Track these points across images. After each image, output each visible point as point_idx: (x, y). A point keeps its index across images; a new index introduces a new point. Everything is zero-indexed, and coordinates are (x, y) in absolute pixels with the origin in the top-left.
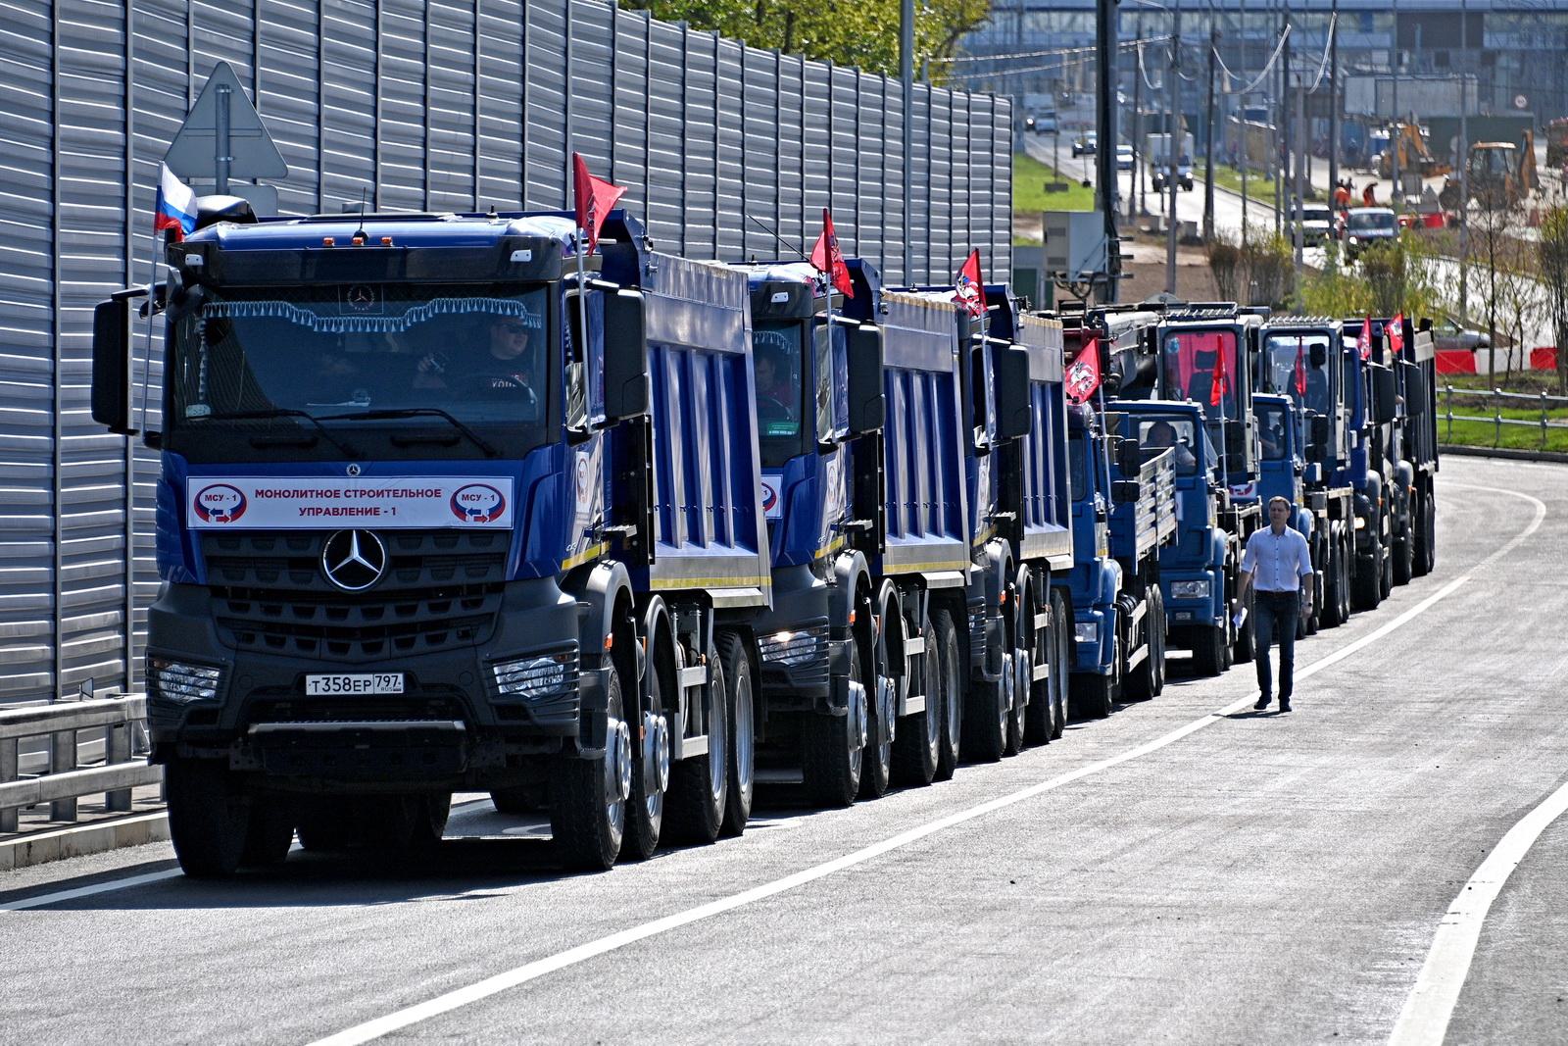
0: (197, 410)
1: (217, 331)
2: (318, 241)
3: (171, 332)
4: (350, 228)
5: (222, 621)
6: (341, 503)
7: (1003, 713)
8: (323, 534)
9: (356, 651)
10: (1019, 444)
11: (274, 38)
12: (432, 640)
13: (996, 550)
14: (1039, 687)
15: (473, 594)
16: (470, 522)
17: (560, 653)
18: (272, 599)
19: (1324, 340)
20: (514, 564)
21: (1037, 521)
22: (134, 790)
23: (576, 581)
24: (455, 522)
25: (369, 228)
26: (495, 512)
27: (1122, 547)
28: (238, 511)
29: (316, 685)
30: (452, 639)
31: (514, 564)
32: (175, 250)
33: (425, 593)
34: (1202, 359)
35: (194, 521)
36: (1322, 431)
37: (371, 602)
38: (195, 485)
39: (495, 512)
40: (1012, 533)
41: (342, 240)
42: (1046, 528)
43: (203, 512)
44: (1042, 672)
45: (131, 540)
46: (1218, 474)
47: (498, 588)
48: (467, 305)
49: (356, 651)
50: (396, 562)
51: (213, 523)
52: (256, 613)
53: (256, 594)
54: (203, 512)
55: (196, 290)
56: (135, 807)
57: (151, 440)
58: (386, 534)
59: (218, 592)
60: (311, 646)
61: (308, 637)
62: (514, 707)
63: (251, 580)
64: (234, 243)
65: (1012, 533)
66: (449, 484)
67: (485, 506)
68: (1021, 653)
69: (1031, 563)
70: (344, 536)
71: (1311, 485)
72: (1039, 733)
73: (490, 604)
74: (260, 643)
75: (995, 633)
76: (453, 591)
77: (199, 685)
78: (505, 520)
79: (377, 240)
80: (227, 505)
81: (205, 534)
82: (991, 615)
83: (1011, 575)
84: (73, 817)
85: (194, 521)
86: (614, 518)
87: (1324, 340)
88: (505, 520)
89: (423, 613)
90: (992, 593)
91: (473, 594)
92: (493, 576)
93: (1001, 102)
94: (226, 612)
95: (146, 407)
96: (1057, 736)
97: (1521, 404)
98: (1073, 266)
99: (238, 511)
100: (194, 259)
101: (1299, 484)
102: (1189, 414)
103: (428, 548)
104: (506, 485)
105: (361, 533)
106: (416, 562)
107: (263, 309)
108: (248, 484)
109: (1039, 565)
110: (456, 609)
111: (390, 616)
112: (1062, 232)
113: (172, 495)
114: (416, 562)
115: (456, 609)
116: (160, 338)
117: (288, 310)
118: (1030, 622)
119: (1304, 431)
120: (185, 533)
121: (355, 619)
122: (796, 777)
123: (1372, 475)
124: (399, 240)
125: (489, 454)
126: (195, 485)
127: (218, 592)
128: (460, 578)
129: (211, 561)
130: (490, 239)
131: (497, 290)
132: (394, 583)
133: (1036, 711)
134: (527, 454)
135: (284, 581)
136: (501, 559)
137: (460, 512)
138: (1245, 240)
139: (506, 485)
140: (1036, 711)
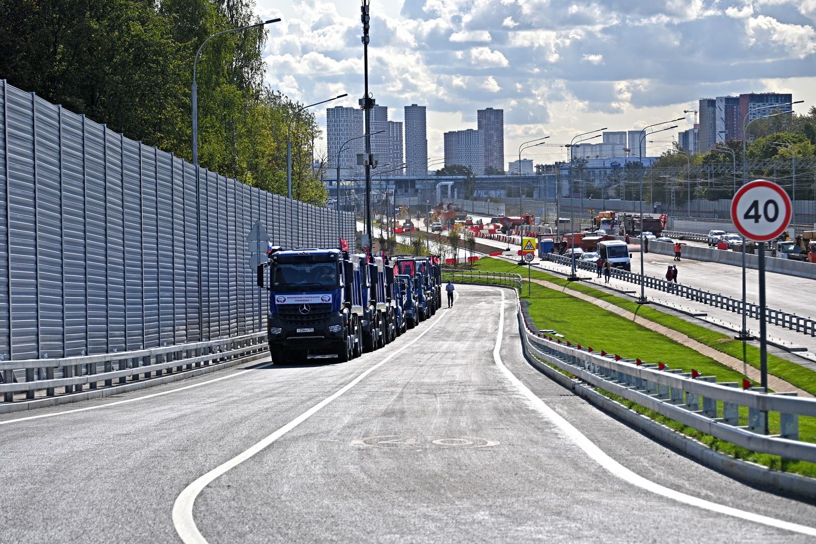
0: (276, 284)
1: (279, 270)
2: (297, 254)
3: (271, 270)
4: (302, 252)
5: (282, 320)
6: (302, 299)
7: (348, 350)
8: (299, 304)
9: (305, 325)
10: (350, 286)
11: (146, 199)
12: (296, 324)
13: (371, 307)
14: (356, 344)
15: (325, 314)
16: (325, 302)
17: (340, 324)
18: (290, 316)
19: (425, 261)
20: (332, 309)
21: (354, 304)
22: (55, 389)
23: (342, 312)
24: (322, 302)
25: (305, 252)
26: (329, 300)
27: (401, 305)
28: (284, 301)
29: (298, 331)
30: (322, 322)
31: (332, 309)
32: (270, 255)
33: (317, 314)
34: (406, 266)
35: (277, 303)
36: (427, 279)
37: (308, 316)
38: (277, 297)
39: (329, 300)
40: (374, 304)
41: (300, 254)
42: (357, 306)
43: (278, 301)
44: (357, 340)
45: (65, 322)
46: (413, 289)
47: (329, 313)
48: (323, 265)
49: (305, 325)
50: (312, 309)
51: (280, 303)
52: (288, 319)
53: (288, 315)
54: (278, 301)
55: (276, 263)
56: (140, 379)
57: (268, 289)
58: (310, 304)
59: (281, 315)
60: (297, 324)
61: (297, 322)
62: (333, 334)
63: (287, 313)
64: (281, 255)
65: (374, 304)
66: (321, 296)
67: (327, 299)
68: (352, 336)
69: (353, 314)
70: (303, 304)
71: (425, 291)
72: (356, 355)
73: (328, 316)
74: (289, 324)
75: (346, 331)
76: (322, 314)
77: (278, 331)
78: (331, 301)
79: (307, 254)
80: (282, 300)
81: (278, 305)
82: (345, 326)
83: (374, 313)
84: (125, 382)
85: (277, 303)
86: (372, 299)
87: (425, 261)
88: (331, 301)
89: (317, 318)
90: (371, 317)
91: (325, 314)
92: (329, 311)
93: (353, 214)
94: (283, 318)
95: (267, 282)
96: (360, 356)
97: (447, 271)
98: (363, 245)
99: (284, 301)
100: (275, 258)
101: (423, 290)
102: (407, 277)
103: (317, 307)
104: (330, 295)
105: (306, 304)
106: (315, 309)
107: (287, 266)
108: (286, 296)
109: (355, 315)
110: (322, 317)
111: (311, 319)
112: (360, 239)
113: (272, 298)
114: (315, 309)
115: (322, 317)
116: (269, 271)
117: (292, 266)
118: (378, 323)
119: (424, 280)
120: (275, 305)
121: (305, 319)
122: (336, 356)
123: (433, 288)
124: (310, 254)
125: (328, 290)
126: (277, 297)
127: (281, 315)
128: (323, 312)
129: (280, 310)
130: (326, 253)
131: (328, 262)
132: (312, 313)
133: (355, 350)
134: (334, 290)
135: (293, 313)
136: (330, 308)
137: (323, 300)
138: (388, 237)
139: (330, 295)
140: (355, 350)
